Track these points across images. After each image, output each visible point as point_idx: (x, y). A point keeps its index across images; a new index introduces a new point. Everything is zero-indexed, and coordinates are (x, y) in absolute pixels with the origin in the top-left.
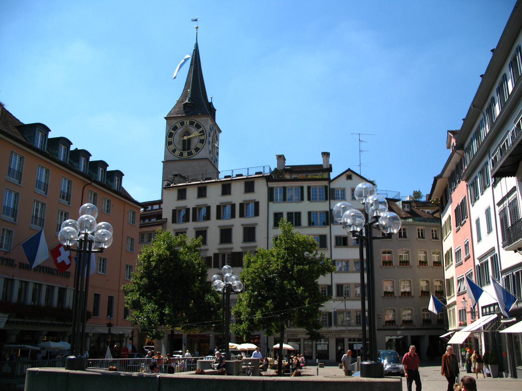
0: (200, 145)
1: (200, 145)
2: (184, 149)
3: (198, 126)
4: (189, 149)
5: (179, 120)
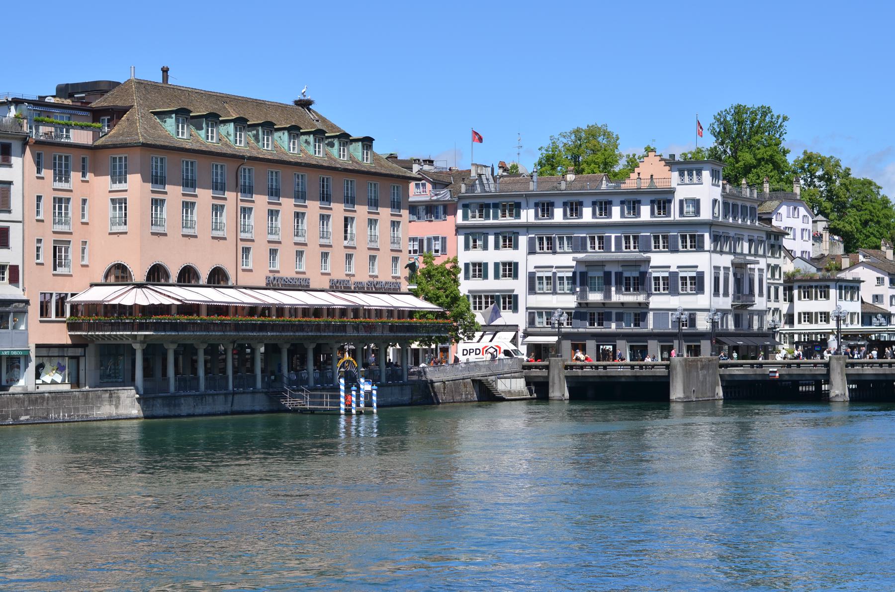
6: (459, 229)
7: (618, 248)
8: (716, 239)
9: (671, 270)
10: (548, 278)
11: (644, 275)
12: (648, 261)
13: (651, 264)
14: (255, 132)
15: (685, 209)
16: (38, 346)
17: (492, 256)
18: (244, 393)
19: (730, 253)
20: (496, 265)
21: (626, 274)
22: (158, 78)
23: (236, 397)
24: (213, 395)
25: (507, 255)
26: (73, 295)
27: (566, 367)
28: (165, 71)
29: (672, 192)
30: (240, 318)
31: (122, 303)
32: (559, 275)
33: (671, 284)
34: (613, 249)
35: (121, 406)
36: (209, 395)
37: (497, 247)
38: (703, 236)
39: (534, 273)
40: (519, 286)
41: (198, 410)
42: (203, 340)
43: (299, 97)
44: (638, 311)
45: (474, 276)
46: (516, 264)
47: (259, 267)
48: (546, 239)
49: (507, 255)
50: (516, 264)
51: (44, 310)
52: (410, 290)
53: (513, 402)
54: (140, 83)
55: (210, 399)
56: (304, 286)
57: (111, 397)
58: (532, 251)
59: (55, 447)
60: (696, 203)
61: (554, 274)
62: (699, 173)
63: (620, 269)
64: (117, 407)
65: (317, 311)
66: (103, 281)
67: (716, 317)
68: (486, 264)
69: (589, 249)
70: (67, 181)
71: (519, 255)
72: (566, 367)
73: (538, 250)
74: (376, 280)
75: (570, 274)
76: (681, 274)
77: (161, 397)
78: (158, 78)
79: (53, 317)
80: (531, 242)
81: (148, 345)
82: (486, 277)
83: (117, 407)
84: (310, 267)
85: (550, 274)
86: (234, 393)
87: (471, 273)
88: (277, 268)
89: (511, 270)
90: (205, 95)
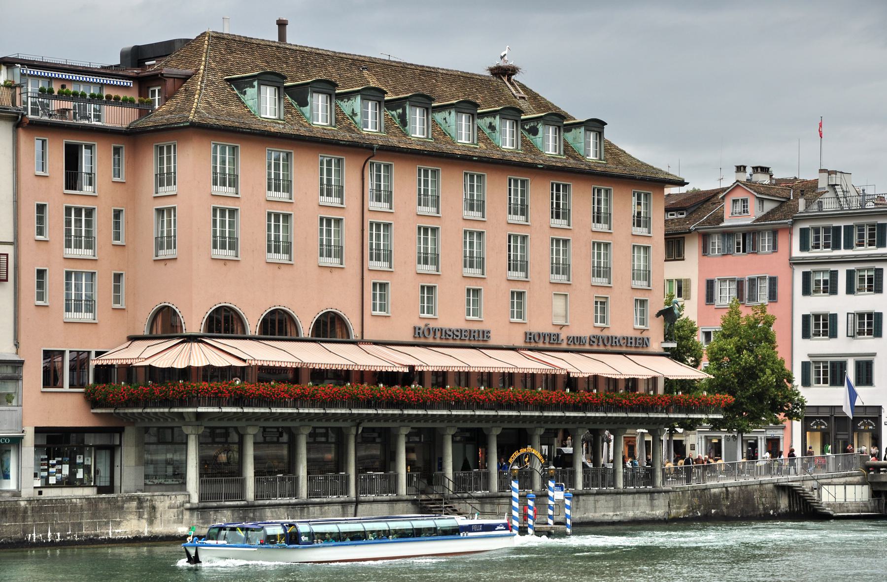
6: (795, 263)
14: (400, 111)
22: (272, 36)
24: (321, 504)
26: (98, 354)
31: (153, 365)
35: (158, 521)
36: (315, 504)
37: (850, 290)
43: (497, 62)
45: (817, 334)
47: (404, 317)
51: (51, 378)
52: (666, 349)
54: (219, 38)
57: (140, 506)
64: (151, 522)
66: (146, 333)
68: (834, 317)
78: (272, 36)
79: (66, 388)
82: (834, 335)
83: (151, 522)
84: (495, 318)
86: (357, 502)
87: (812, 329)
90: (332, 57)
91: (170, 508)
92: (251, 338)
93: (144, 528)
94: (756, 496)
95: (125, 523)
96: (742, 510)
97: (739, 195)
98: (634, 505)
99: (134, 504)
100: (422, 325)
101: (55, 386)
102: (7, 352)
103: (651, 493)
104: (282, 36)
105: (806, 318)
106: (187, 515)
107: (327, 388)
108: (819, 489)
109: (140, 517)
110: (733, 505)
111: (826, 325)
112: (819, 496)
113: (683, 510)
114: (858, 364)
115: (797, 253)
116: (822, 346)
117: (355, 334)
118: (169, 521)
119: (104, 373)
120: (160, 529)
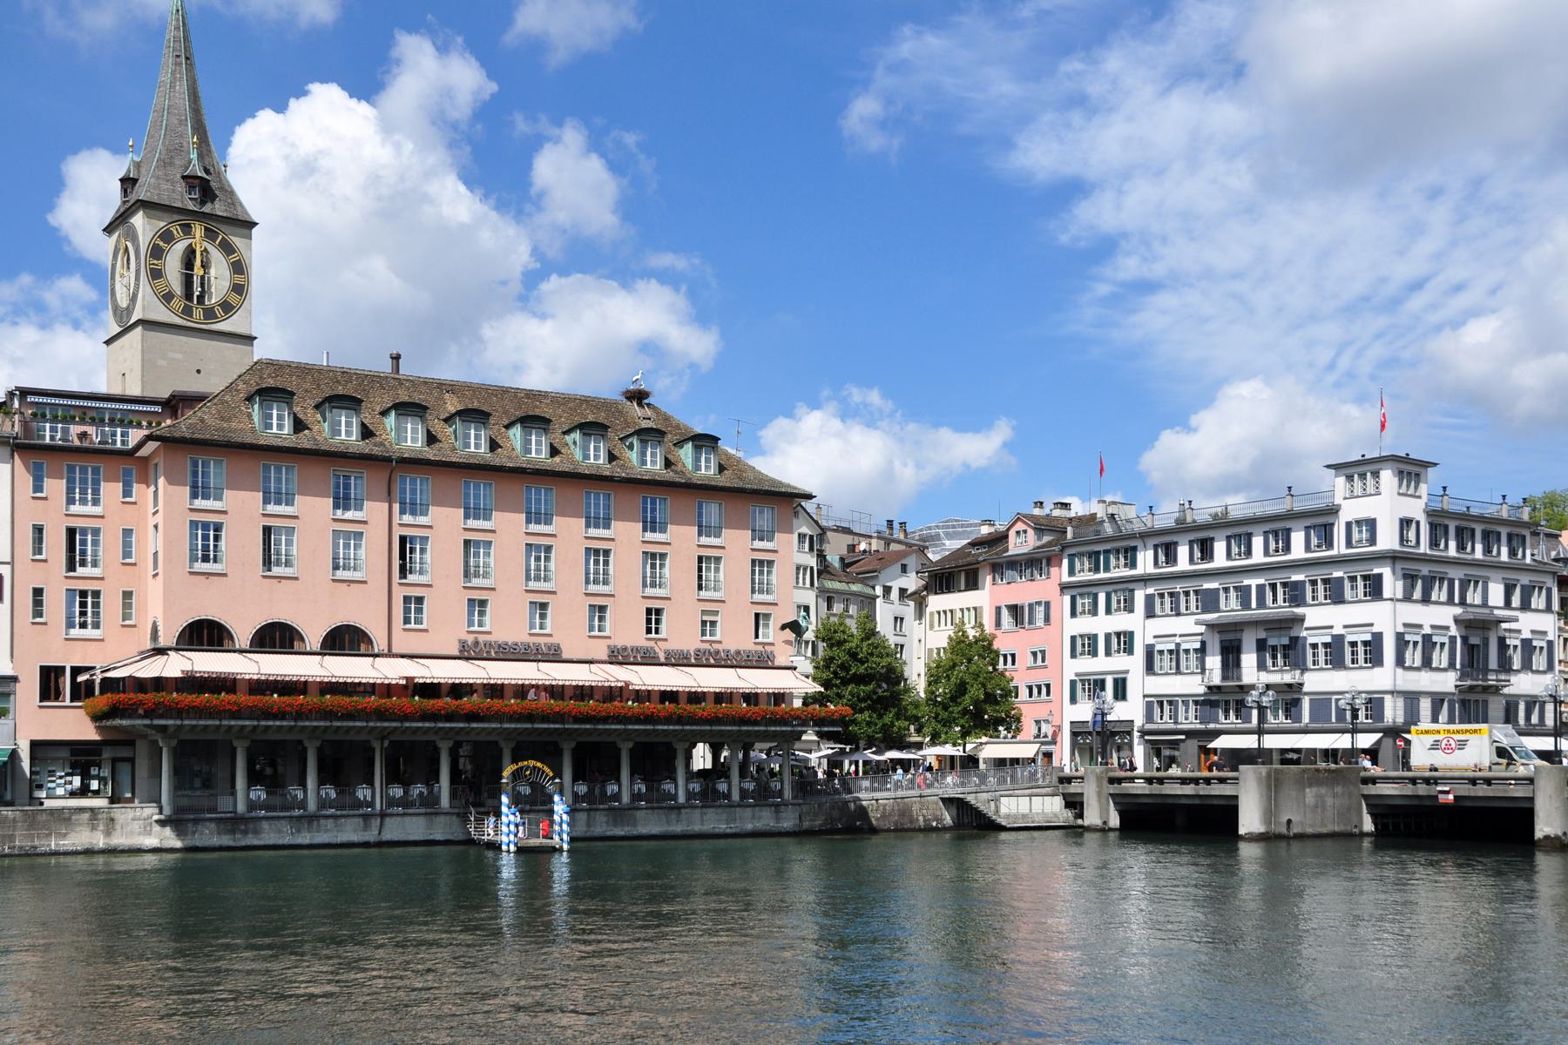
0: (234, 299)
1: (234, 299)
2: (188, 295)
3: (227, 249)
4: (201, 299)
5: (176, 217)
6: (1064, 588)
7: (1261, 603)
8: (1410, 578)
9: (1335, 632)
10: (1171, 652)
11: (1295, 642)
12: (1301, 619)
13: (1306, 624)
15: (1355, 536)
16: (35, 745)
17: (1102, 624)
18: (404, 814)
19: (1450, 601)
20: (1108, 637)
21: (1271, 642)
22: (386, 367)
23: (387, 820)
25: (1121, 622)
27: (1112, 781)
28: (396, 358)
29: (1334, 511)
30: (131, 695)
32: (1184, 646)
33: (1336, 653)
34: (1254, 605)
36: (327, 817)
38: (1380, 576)
39: (1153, 646)
40: (1133, 664)
41: (299, 840)
42: (383, 735)
44: (1289, 697)
46: (1132, 634)
48: (1169, 594)
49: (1121, 622)
50: (1132, 634)
53: (1036, 834)
55: (330, 823)
56: (553, 655)
58: (1150, 614)
59: (898, 861)
60: (1371, 524)
61: (1178, 645)
62: (1376, 474)
63: (1262, 635)
64: (108, 833)
65: (582, 692)
67: (1264, 699)
69: (1222, 606)
70: (96, 502)
71: (1131, 621)
72: (1112, 781)
73: (1183, 610)
74: (716, 646)
75: (1198, 645)
76: (1350, 638)
77: (211, 820)
78: (386, 367)
79: (68, 703)
80: (1149, 600)
81: (182, 743)
82: (1094, 653)
83: (108, 833)
85: (1172, 647)
86: (383, 815)
88: (717, 638)
89: (1125, 641)
91: (134, 819)
92: (241, 651)
93: (100, 841)
94: (915, 808)
95: (73, 835)
96: (896, 823)
97: (1020, 526)
98: (753, 817)
99: (87, 816)
100: (470, 639)
101: (57, 699)
102: (7, 670)
103: (777, 805)
104: (397, 369)
105: (1073, 638)
106: (157, 828)
107: (151, 697)
108: (996, 800)
109: (94, 828)
110: (884, 816)
111: (1087, 645)
112: (997, 811)
113: (818, 822)
114: (1116, 681)
115: (1066, 578)
116: (1087, 665)
117: (380, 644)
118: (132, 833)
119: (109, 685)
120: (118, 840)
